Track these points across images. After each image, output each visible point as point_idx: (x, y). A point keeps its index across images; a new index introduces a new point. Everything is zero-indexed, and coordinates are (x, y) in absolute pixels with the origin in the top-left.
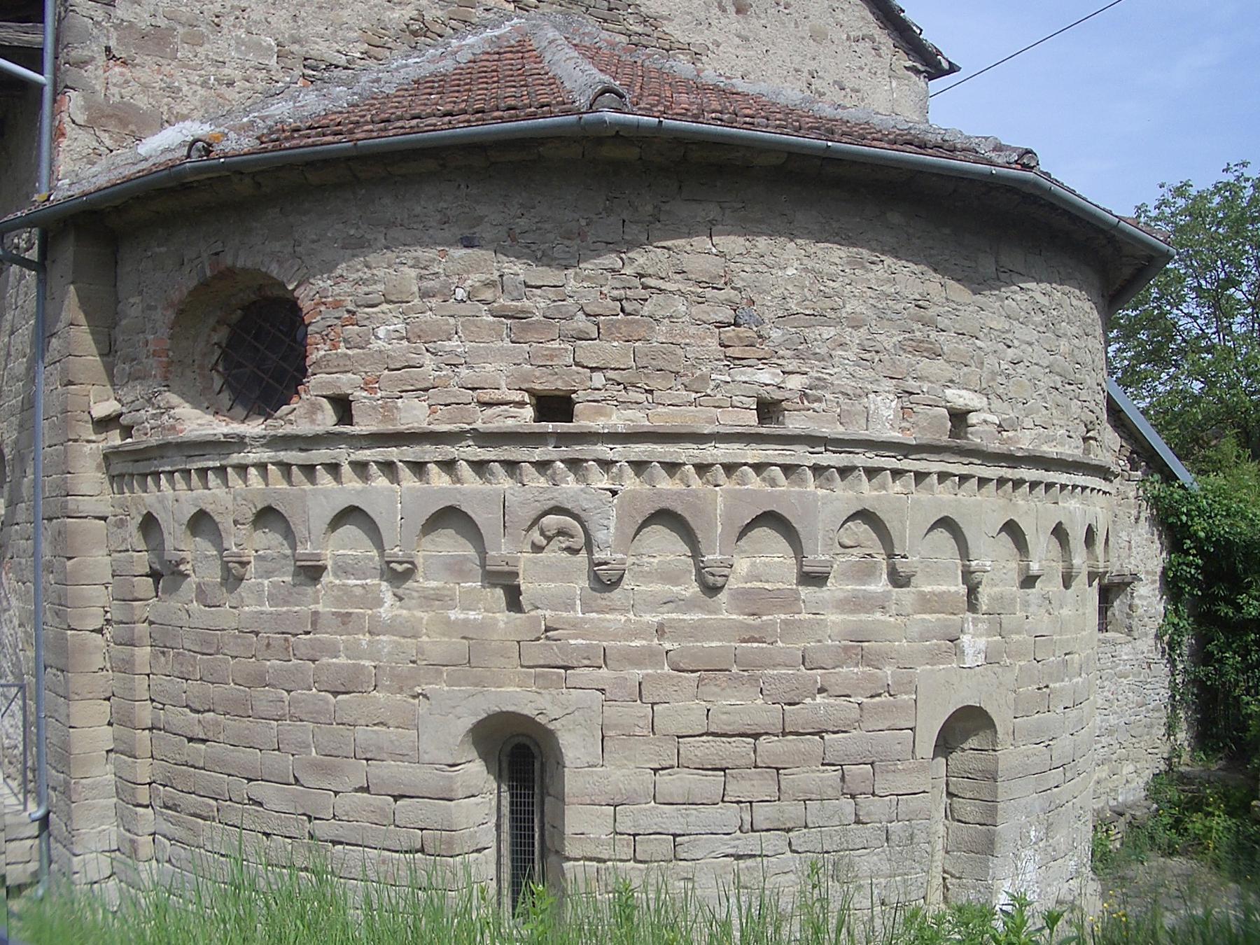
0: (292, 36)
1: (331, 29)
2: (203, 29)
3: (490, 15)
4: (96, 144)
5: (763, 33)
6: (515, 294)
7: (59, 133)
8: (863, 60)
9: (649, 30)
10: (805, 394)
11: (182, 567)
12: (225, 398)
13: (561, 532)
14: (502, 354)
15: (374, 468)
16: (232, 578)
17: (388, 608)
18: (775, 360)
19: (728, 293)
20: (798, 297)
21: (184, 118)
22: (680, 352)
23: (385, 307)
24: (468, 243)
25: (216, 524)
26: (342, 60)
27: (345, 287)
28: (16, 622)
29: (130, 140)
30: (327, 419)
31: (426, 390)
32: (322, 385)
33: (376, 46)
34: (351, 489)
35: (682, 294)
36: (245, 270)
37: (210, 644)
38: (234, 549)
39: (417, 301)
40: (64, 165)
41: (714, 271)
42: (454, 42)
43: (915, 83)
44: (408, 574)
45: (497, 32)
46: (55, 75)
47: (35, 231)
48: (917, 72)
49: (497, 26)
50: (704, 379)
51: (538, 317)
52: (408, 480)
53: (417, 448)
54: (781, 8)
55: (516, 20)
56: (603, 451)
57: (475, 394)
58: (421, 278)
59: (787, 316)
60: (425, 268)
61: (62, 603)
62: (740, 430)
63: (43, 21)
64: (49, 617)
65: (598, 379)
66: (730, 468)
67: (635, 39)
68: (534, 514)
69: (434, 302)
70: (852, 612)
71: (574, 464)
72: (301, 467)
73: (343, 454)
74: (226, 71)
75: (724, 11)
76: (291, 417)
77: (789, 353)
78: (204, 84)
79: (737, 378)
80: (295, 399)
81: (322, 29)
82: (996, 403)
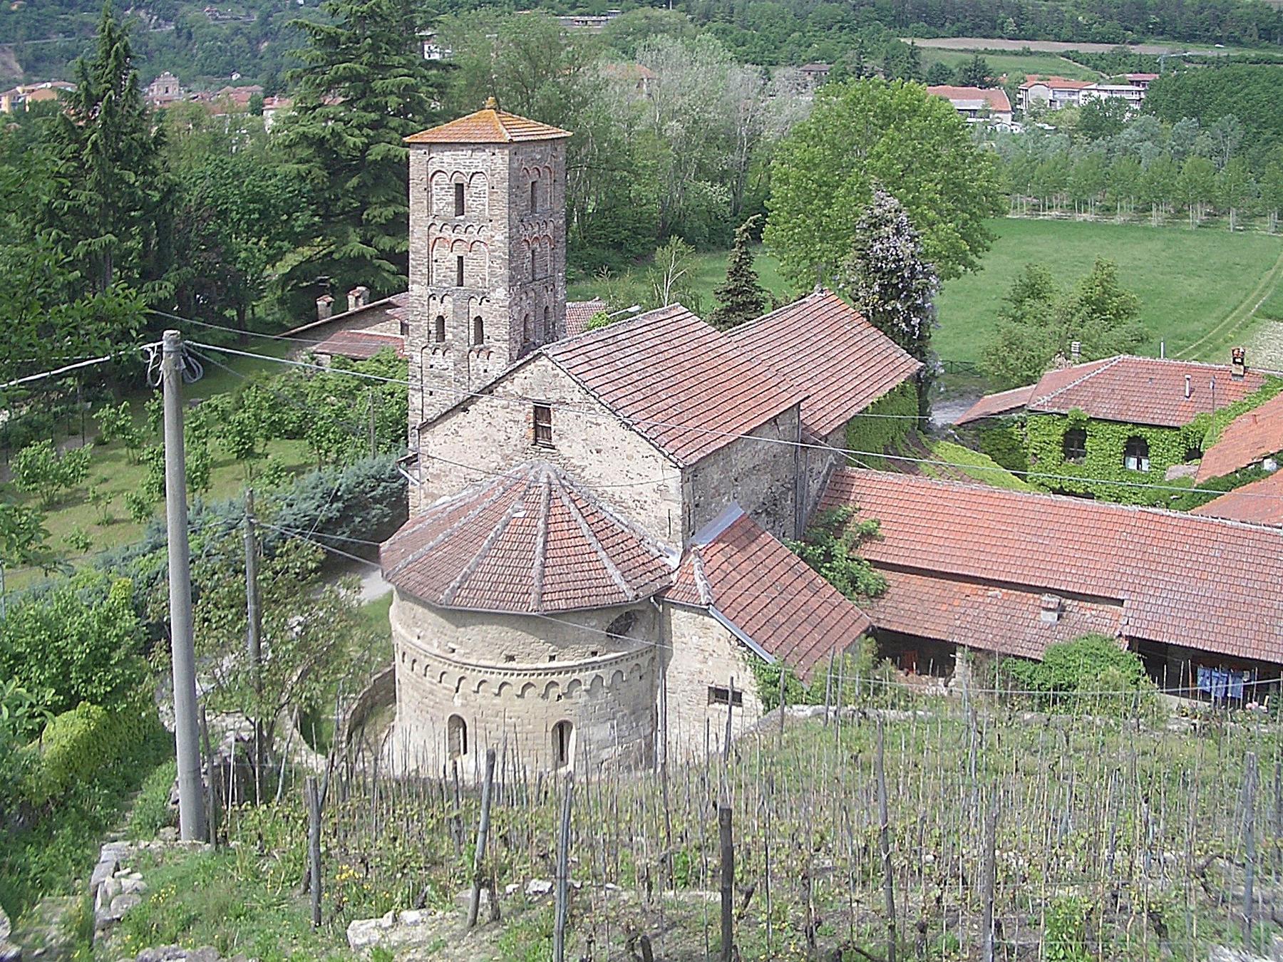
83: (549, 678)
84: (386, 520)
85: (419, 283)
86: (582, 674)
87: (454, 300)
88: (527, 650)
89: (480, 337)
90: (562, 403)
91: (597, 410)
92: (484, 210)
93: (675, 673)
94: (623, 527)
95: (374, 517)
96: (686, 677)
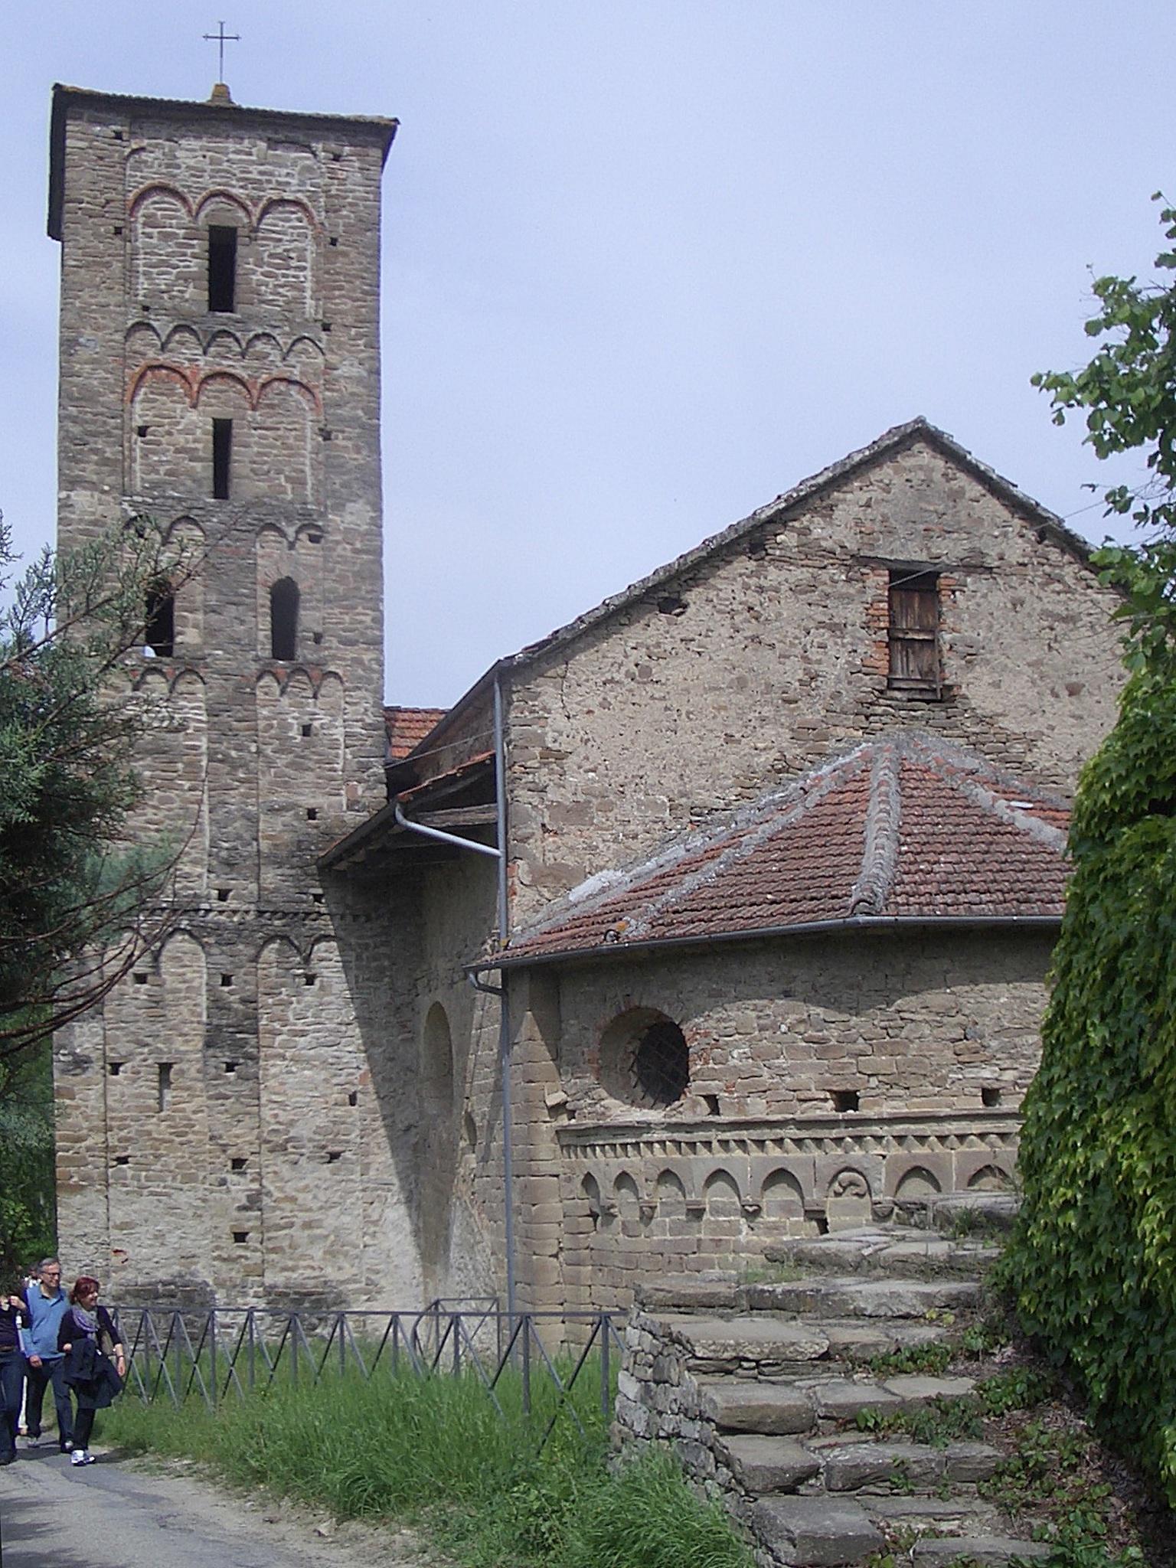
0: (679, 791)
1: (710, 780)
2: (611, 797)
3: (841, 745)
4: (538, 897)
5: (1097, 709)
6: (819, 1028)
7: (511, 892)
9: (985, 728)
10: (1017, 1083)
11: (612, 1211)
12: (639, 1091)
13: (852, 1184)
14: (812, 1067)
15: (732, 1144)
16: (647, 1216)
17: (745, 1236)
18: (994, 1061)
19: (960, 1018)
20: (1009, 1017)
21: (602, 868)
22: (927, 1061)
23: (737, 1037)
24: (787, 994)
25: (634, 1182)
26: (721, 804)
27: (712, 1023)
28: (488, 1251)
29: (562, 891)
30: (703, 1113)
31: (765, 1092)
32: (704, 1088)
33: (747, 787)
34: (717, 1158)
35: (927, 1022)
36: (647, 1008)
37: (631, 1262)
38: (646, 1198)
39: (757, 1033)
40: (516, 915)
41: (948, 1005)
42: (812, 774)
44: (757, 1213)
45: (848, 759)
46: (506, 848)
47: (499, 971)
49: (847, 752)
50: (945, 1078)
51: (833, 1042)
52: (755, 1152)
53: (759, 1131)
54: (1115, 681)
55: (864, 745)
56: (876, 1130)
57: (795, 1094)
58: (759, 1017)
59: (1002, 1031)
60: (761, 1011)
61: (528, 1238)
62: (965, 1112)
63: (496, 802)
64: (519, 1246)
65: (874, 1082)
66: (961, 1138)
67: (973, 739)
68: (833, 1173)
69: (767, 1034)
71: (858, 1139)
72: (687, 1143)
73: (713, 1135)
74: (632, 827)
75: (1057, 696)
76: (681, 1109)
77: (1004, 1055)
78: (615, 841)
79: (967, 1076)
80: (683, 1097)
81: (703, 782)
85: (93, 486)
89: (284, 642)
90: (976, 566)
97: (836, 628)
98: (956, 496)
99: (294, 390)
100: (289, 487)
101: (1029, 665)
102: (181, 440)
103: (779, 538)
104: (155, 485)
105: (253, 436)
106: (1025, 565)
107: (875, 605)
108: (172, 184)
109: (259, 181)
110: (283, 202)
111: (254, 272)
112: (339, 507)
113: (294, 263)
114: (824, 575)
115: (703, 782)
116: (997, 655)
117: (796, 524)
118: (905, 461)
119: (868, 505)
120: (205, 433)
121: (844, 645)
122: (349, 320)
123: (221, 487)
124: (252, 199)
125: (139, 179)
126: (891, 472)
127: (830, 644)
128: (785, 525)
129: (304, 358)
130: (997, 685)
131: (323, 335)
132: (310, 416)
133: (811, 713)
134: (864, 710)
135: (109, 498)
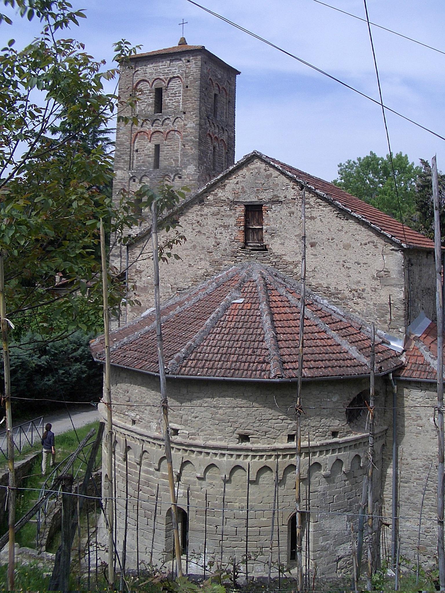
3: (227, 267)
5: (322, 252)
8: (369, 251)
33: (195, 282)
43: (396, 255)
48: (396, 251)
70: (147, 474)
82: (188, 428)
83: (288, 461)
84: (84, 376)
85: (122, 169)
86: (323, 456)
87: (151, 179)
88: (264, 428)
90: (275, 201)
91: (312, 203)
92: (179, 106)
93: (409, 459)
94: (340, 317)
95: (75, 371)
96: (421, 464)
97: (226, 227)
98: (269, 176)
99: (176, 133)
100: (174, 162)
101: (296, 236)
102: (146, 152)
103: (208, 198)
104: (139, 166)
105: (164, 148)
106: (295, 199)
107: (239, 218)
108: (145, 79)
109: (168, 73)
110: (174, 77)
111: (166, 100)
112: (186, 168)
113: (178, 95)
114: (222, 209)
115: (181, 280)
116: (283, 233)
117: (213, 193)
118: (251, 166)
119: (237, 183)
120: (153, 149)
121: (228, 232)
122: (191, 109)
123: (157, 165)
124: (165, 78)
125: (137, 79)
126: (246, 171)
127: (224, 232)
128: (210, 193)
129: (178, 123)
130: (283, 244)
131: (183, 116)
132: (180, 140)
133: (217, 256)
134: (234, 254)
135: (125, 172)
